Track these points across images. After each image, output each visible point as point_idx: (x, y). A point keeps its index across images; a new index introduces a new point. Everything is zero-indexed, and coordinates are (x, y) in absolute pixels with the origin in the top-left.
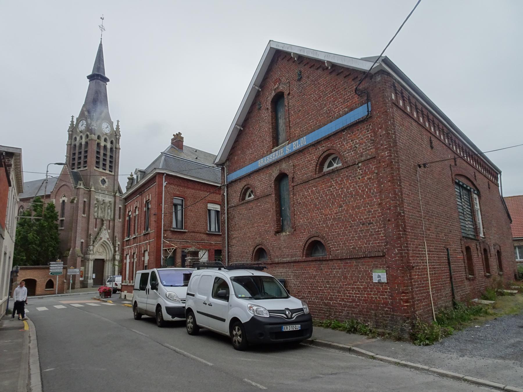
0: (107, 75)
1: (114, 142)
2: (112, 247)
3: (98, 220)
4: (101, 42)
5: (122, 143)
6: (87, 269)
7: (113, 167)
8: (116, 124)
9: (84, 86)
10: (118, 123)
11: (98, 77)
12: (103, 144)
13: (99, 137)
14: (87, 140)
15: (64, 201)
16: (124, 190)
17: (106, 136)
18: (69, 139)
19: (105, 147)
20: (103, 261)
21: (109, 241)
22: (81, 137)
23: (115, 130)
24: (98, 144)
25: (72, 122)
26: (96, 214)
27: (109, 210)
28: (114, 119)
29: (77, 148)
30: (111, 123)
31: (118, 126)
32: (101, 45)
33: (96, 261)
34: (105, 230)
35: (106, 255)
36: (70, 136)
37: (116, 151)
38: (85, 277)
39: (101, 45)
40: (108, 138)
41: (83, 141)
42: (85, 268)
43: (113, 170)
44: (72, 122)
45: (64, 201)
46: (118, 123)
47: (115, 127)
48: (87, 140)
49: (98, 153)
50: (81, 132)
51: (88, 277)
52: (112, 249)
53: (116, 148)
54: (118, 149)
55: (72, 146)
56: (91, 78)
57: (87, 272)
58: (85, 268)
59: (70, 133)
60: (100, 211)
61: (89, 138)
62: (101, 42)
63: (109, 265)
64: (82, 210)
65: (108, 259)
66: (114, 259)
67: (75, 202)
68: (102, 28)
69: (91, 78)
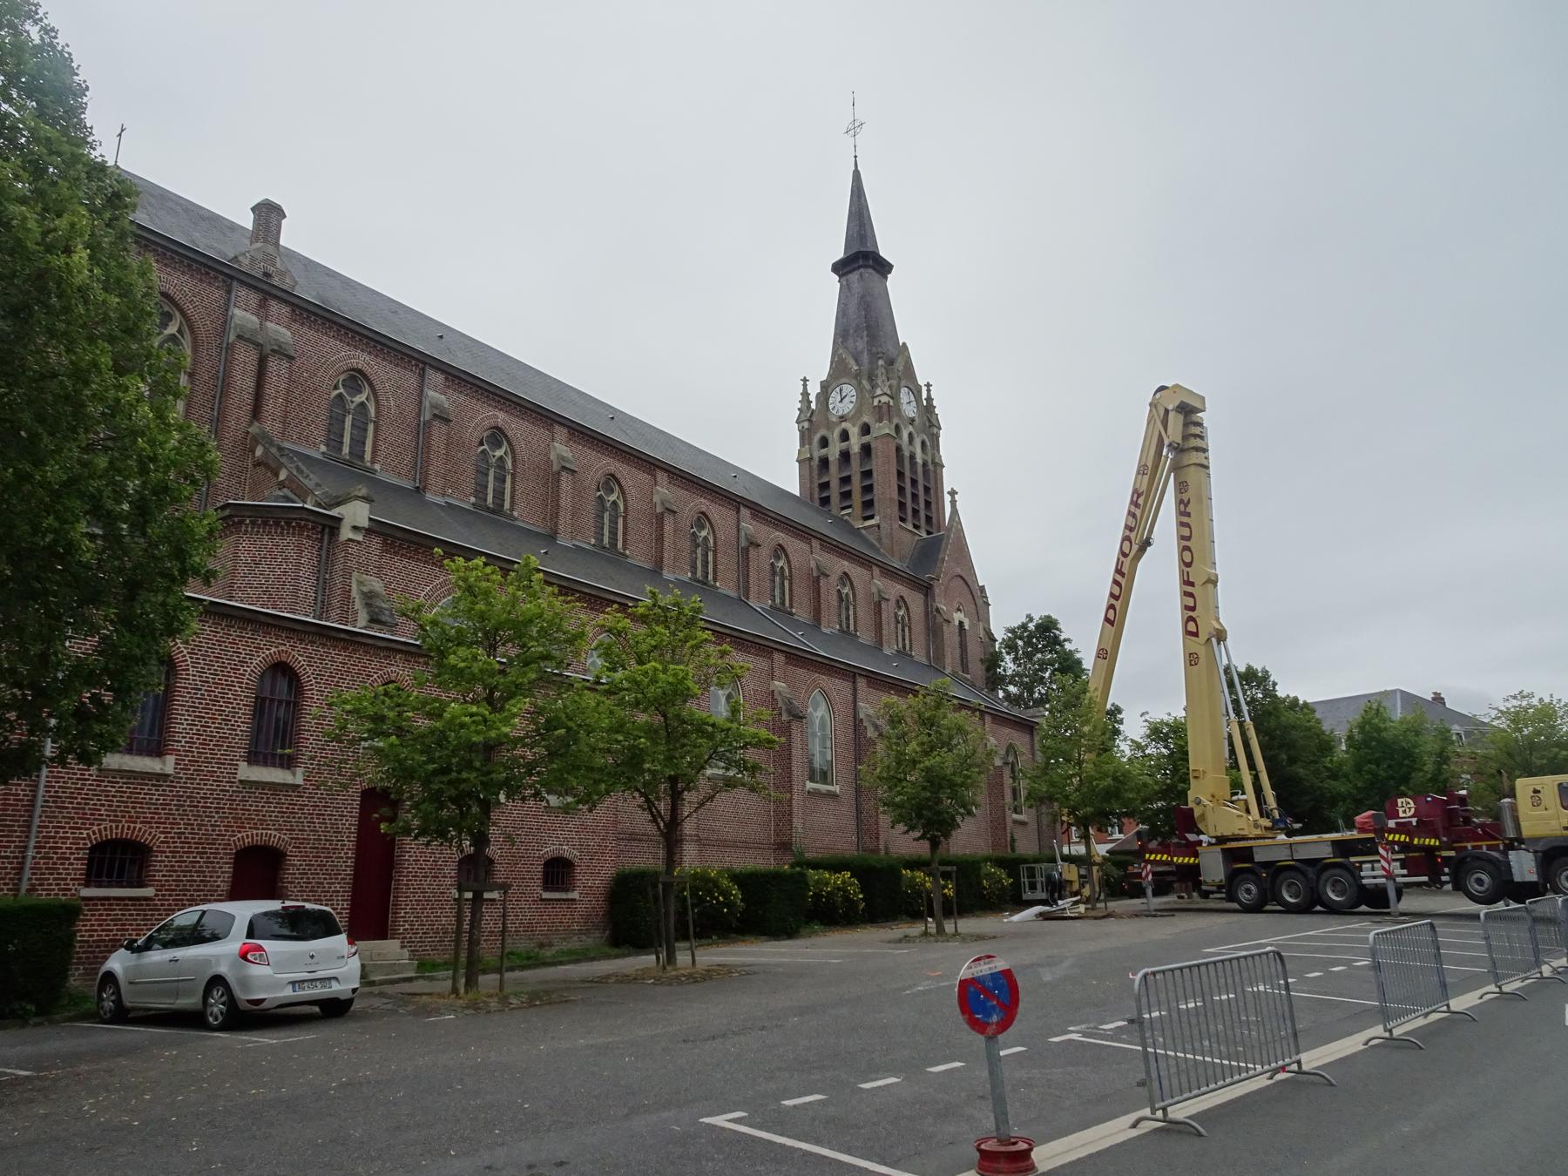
0: (884, 253)
9: (825, 296)
10: (805, 386)
11: (862, 262)
14: (866, 439)
18: (802, 444)
22: (845, 436)
25: (805, 394)
29: (833, 468)
32: (857, 175)
36: (805, 437)
39: (857, 175)
41: (855, 444)
44: (805, 394)
46: (805, 386)
48: (866, 439)
50: (843, 418)
53: (934, 463)
54: (939, 466)
55: (816, 462)
56: (840, 268)
59: (806, 425)
61: (874, 433)
64: (248, 398)
69: (840, 268)
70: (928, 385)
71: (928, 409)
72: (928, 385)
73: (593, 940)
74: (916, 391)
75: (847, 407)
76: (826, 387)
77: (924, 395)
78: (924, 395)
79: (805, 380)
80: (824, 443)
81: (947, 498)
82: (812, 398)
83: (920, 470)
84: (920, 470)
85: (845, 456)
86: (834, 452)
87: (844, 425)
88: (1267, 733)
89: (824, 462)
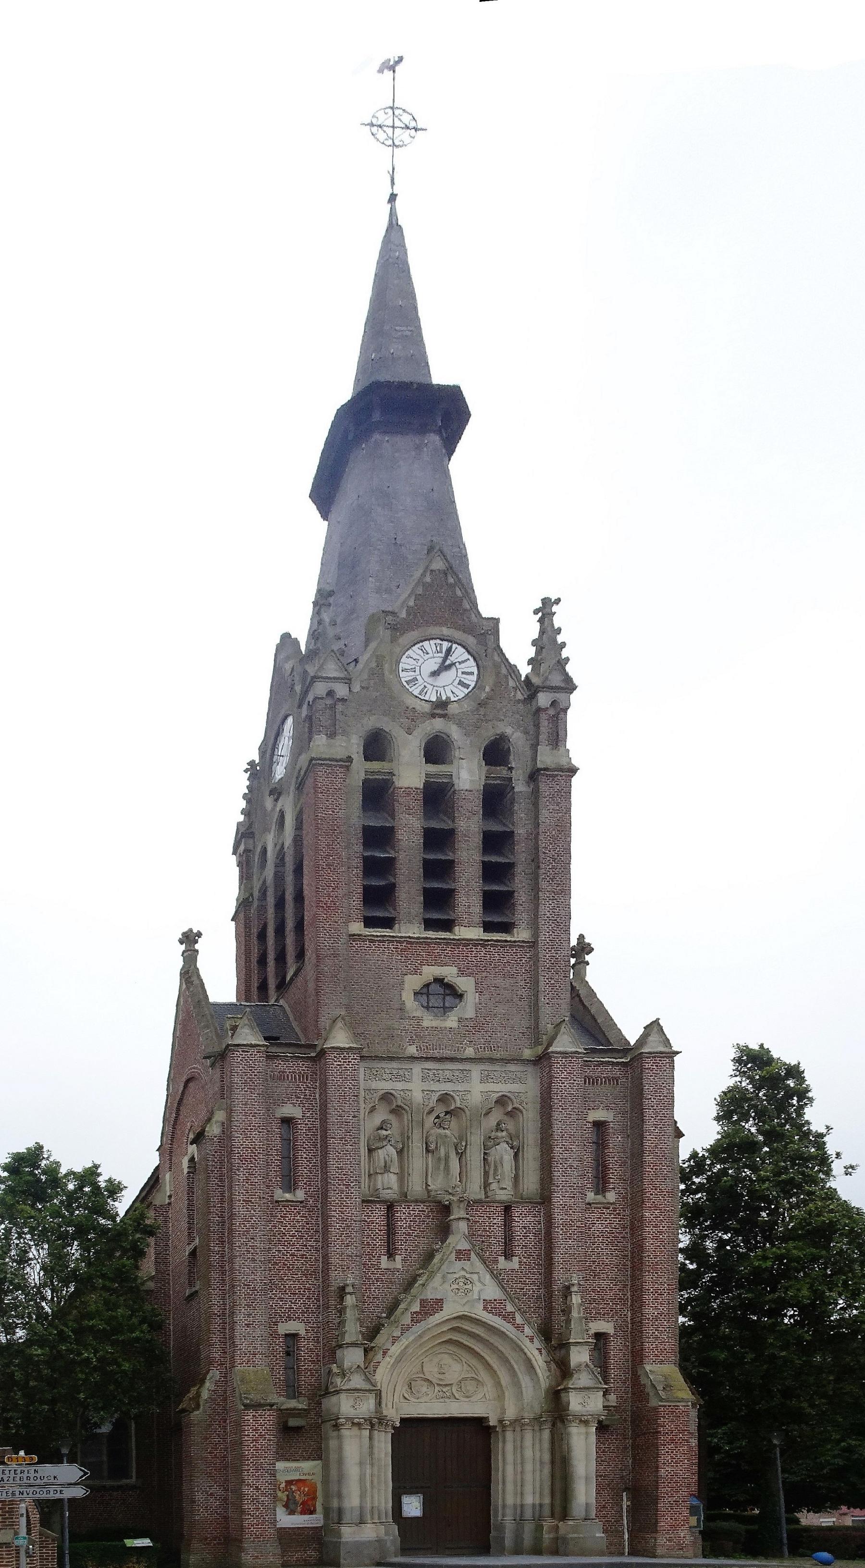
1: (517, 739)
2: (535, 1351)
3: (402, 1213)
4: (393, 214)
5: (587, 733)
6: (334, 1473)
7: (522, 898)
8: (534, 630)
12: (410, 773)
13: (376, 746)
15: (391, 1255)
16: (303, 648)
17: (438, 724)
19: (437, 796)
20: (478, 1433)
21: (508, 1317)
23: (525, 670)
24: (377, 794)
26: (392, 1180)
27: (503, 1152)
28: (503, 594)
30: (484, 636)
31: (548, 643)
32: (394, 229)
33: (412, 1434)
34: (462, 1255)
35: (501, 1397)
37: (535, 794)
38: (327, 1511)
39: (394, 229)
40: (455, 733)
42: (326, 1468)
43: (521, 915)
45: (391, 1255)
47: (518, 647)
49: (378, 837)
51: (340, 1511)
52: (539, 1361)
57: (334, 1487)
58: (326, 1468)
60: (417, 1161)
62: (393, 214)
63: (520, 1448)
65: (511, 1413)
66: (556, 1412)
67: (214, 1130)
68: (395, 126)
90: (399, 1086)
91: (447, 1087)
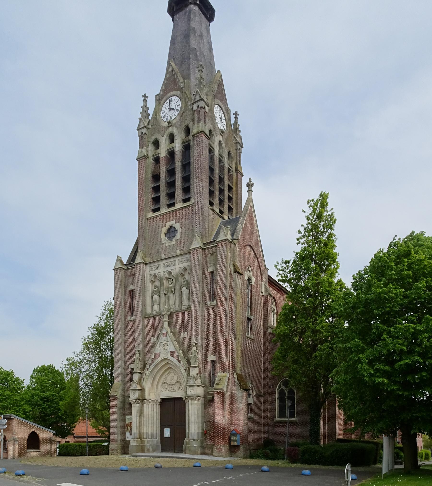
10: (145, 100)
22: (172, 138)
25: (145, 108)
29: (163, 163)
53: (237, 170)
70: (236, 114)
71: (235, 130)
72: (236, 114)
73: (224, 454)
74: (226, 111)
75: (173, 116)
76: (160, 99)
77: (233, 121)
78: (233, 121)
79: (145, 97)
80: (156, 144)
81: (245, 189)
82: (151, 111)
83: (226, 171)
84: (226, 171)
85: (171, 154)
86: (163, 153)
87: (170, 129)
88: (32, 419)
89: (157, 160)
90: (157, 271)
91: (169, 269)
